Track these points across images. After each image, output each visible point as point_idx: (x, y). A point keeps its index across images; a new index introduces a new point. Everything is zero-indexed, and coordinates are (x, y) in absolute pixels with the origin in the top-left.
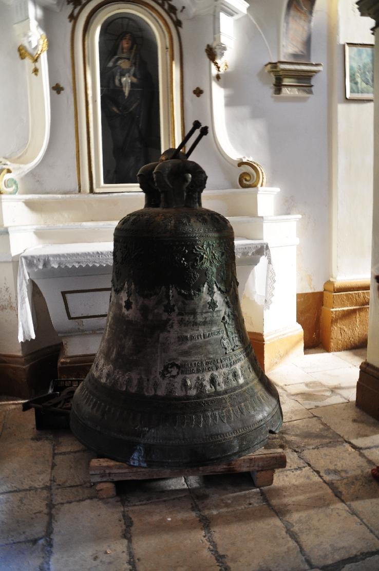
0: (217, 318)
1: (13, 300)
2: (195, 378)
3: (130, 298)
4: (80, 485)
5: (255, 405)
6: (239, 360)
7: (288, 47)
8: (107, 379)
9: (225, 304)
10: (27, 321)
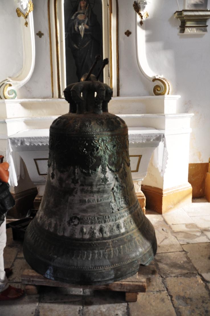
0: (108, 189)
2: (89, 228)
3: (54, 172)
6: (123, 216)
9: (114, 180)
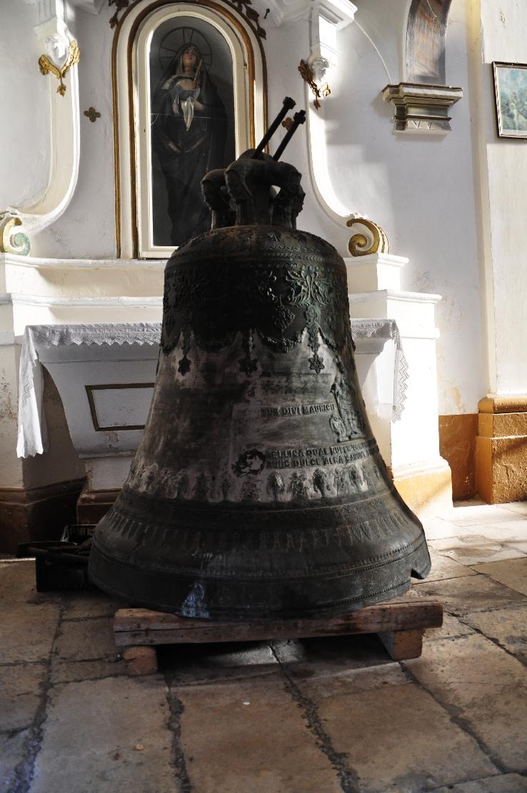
1: (13, 403)
4: (98, 660)
5: (387, 528)
7: (414, 66)
8: (148, 484)
9: (335, 367)
10: (31, 426)
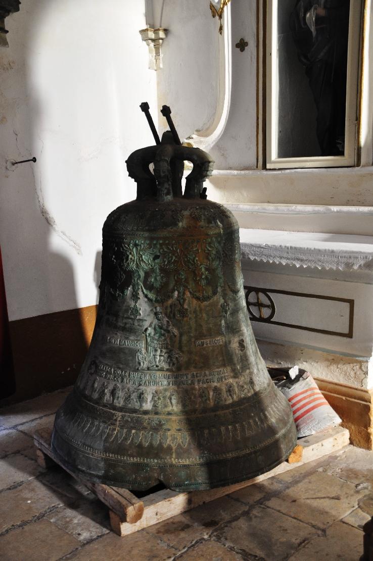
9: (152, 315)
